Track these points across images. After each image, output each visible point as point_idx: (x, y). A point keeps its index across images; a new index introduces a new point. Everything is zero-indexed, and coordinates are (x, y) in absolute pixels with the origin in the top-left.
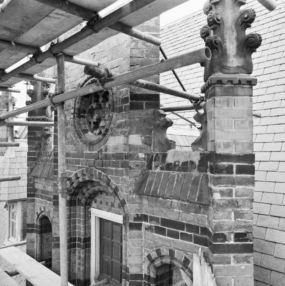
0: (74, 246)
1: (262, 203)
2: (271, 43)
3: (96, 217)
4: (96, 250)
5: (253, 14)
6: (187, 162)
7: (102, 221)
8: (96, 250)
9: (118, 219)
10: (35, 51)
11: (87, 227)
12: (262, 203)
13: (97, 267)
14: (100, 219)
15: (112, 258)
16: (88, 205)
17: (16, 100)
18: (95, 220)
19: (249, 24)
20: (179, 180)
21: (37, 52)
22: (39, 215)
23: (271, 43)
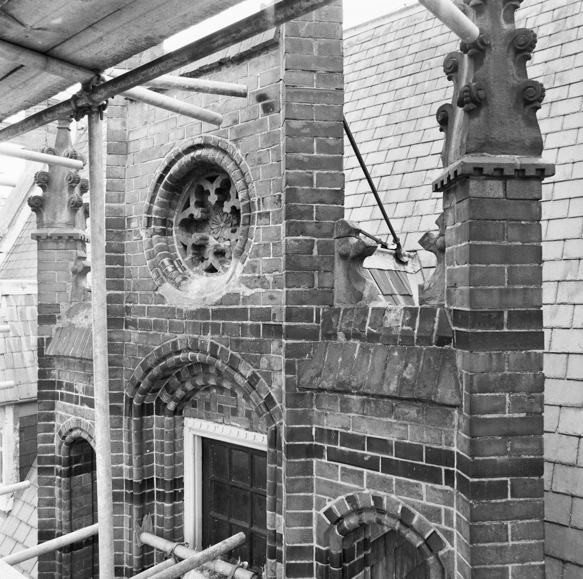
0: (151, 496)
1: (568, 379)
2: (410, 145)
3: (194, 435)
4: (195, 494)
5: (533, 39)
6: (108, 306)
7: (208, 445)
8: (195, 494)
9: (258, 441)
10: (87, 76)
11: (177, 460)
12: (568, 379)
13: (197, 522)
14: (203, 438)
15: (252, 526)
16: (177, 412)
17: (82, 132)
18: (193, 442)
19: (527, 53)
20: (396, 354)
21: (93, 78)
22: (64, 438)
23: (410, 145)
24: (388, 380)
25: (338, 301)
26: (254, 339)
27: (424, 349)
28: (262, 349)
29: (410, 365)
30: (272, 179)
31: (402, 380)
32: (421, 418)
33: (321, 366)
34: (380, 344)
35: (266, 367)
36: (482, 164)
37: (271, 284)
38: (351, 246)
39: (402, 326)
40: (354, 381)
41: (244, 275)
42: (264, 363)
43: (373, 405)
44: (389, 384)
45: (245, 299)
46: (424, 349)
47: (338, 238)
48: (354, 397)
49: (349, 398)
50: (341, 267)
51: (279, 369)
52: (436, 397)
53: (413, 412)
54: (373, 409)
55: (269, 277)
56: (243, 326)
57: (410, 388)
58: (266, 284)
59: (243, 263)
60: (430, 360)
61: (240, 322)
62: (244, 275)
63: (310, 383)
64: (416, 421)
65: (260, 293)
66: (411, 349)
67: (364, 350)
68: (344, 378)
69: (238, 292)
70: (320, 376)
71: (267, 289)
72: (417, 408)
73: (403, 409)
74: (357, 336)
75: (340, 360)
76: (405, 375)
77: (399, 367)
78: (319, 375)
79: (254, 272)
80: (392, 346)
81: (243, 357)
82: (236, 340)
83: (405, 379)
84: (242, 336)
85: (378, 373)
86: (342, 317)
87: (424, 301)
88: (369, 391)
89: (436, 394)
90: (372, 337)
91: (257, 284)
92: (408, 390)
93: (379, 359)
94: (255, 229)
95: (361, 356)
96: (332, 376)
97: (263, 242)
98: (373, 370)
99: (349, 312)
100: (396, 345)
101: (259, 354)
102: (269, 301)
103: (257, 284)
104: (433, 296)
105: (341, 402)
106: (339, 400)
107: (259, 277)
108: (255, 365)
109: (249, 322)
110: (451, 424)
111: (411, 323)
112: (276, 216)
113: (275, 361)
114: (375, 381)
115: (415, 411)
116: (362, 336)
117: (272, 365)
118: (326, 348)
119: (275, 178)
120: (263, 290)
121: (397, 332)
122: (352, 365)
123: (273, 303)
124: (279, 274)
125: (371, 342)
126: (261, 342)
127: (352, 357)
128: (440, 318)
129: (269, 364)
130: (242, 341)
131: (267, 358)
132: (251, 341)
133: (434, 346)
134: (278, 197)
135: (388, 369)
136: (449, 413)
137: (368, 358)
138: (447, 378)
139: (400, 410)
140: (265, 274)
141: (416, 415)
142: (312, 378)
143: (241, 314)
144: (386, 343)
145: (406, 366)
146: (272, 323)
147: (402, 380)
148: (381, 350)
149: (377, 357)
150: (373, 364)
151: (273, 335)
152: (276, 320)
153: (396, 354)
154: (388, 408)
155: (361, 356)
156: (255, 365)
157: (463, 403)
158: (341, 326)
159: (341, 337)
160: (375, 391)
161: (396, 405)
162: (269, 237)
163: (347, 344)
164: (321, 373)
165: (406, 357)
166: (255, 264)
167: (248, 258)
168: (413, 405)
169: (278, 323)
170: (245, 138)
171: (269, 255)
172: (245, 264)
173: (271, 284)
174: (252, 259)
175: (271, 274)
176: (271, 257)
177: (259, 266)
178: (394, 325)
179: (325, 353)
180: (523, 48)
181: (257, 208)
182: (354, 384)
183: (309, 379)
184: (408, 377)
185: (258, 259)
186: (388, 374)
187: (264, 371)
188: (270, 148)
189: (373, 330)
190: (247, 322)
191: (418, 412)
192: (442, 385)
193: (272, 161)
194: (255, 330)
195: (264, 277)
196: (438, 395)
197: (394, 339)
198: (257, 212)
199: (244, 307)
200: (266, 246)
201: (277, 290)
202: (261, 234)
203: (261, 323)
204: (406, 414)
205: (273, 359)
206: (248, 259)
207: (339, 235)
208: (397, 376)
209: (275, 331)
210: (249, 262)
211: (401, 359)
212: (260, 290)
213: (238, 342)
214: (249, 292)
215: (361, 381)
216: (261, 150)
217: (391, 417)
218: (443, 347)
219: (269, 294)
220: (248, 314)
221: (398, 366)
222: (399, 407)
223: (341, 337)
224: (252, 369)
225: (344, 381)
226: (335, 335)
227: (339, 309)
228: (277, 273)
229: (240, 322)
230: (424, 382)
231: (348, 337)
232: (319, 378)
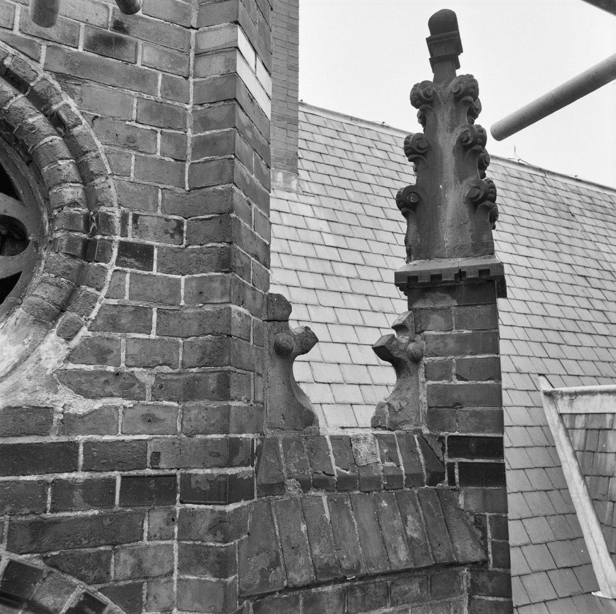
20: (384, 504)
24: (391, 546)
25: (272, 427)
26: (96, 512)
27: (416, 492)
28: (121, 533)
29: (410, 518)
30: (161, 186)
31: (409, 541)
32: (425, 593)
33: (274, 544)
34: (358, 492)
35: (129, 573)
36: (441, 270)
37: (148, 391)
38: (294, 336)
39: (383, 462)
40: (343, 559)
41: (71, 366)
42: (121, 567)
43: (359, 594)
44: (396, 552)
45: (70, 422)
46: (416, 492)
47: (268, 321)
48: (329, 589)
49: (320, 593)
50: (277, 369)
51: (167, 569)
52: (457, 555)
53: (414, 588)
54: (360, 600)
55: (146, 377)
56: (58, 485)
57: (424, 551)
58: (136, 390)
59: (68, 339)
60: (429, 506)
61: (49, 478)
62: (71, 366)
63: (264, 583)
64: (420, 600)
65: (117, 408)
66: (400, 493)
67: (337, 505)
68: (325, 558)
69: (48, 403)
70: (278, 564)
71: (138, 399)
72: (420, 580)
73: (402, 587)
74: (322, 483)
75: (303, 528)
76: (409, 533)
77: (397, 523)
78: (275, 564)
79: (103, 360)
80: (375, 492)
81: (54, 564)
82: (32, 524)
83: (412, 539)
84: (52, 511)
85: (374, 538)
86: (285, 454)
87: (397, 426)
88: (373, 570)
89: (455, 550)
90: (345, 484)
91: (109, 389)
92: (422, 554)
93: (366, 516)
94: (110, 272)
95: (337, 516)
96: (301, 560)
97: (133, 303)
98: (364, 537)
99: (293, 445)
100: (379, 491)
101: (109, 548)
102: (142, 426)
103: (109, 389)
104: (408, 419)
105: (305, 603)
106: (301, 602)
107: (117, 374)
108: (92, 575)
109: (80, 476)
110: (460, 589)
111: (392, 458)
112: (169, 257)
113: (155, 556)
114: (375, 551)
115: (417, 585)
116: (331, 483)
117: (146, 565)
118: (270, 510)
119: (168, 187)
120: (128, 403)
121: (378, 471)
122: (328, 534)
123: (154, 430)
124: (171, 370)
125: (345, 491)
126: (118, 518)
127: (322, 519)
128: (422, 447)
129: (139, 566)
130: (56, 522)
131: (132, 553)
132: (86, 519)
133: (426, 486)
134: (175, 224)
135: (384, 528)
136: (456, 574)
137: (349, 516)
138: (460, 529)
139: (397, 589)
140: (135, 369)
141: (419, 590)
142: (264, 573)
143: (64, 456)
144: (367, 490)
145: (405, 520)
146: (149, 471)
147: (409, 541)
148: (363, 500)
149: (361, 518)
150: (360, 525)
151: (151, 499)
152: (162, 465)
153: (386, 505)
154: (381, 592)
155: (337, 516)
156: (92, 575)
157: (490, 556)
158: (288, 470)
159: (293, 488)
160: (380, 569)
161: (392, 583)
162: (148, 293)
163: (305, 497)
164: (277, 558)
165: (399, 506)
166: (106, 344)
167: (85, 329)
168: (415, 577)
169: (167, 472)
170: (92, 84)
171: (148, 330)
172: (75, 342)
173: (148, 391)
174: (98, 334)
175: (149, 371)
176: (153, 336)
177: (119, 350)
178: (371, 461)
179: (272, 520)
180: (421, 152)
181: (118, 230)
182: (346, 565)
183: (259, 577)
184: (415, 535)
185: (117, 335)
186: (388, 538)
187: (122, 583)
188: (159, 130)
189: (345, 471)
190: (73, 475)
191: (421, 585)
192: (456, 538)
193: (163, 154)
194: (99, 493)
195: (132, 375)
196: (459, 552)
197: (374, 482)
198: (118, 238)
199: (63, 439)
200: (140, 314)
201: (166, 403)
202: (127, 286)
203: (117, 475)
204: (406, 593)
205: (151, 553)
206: (84, 332)
207: (271, 317)
208: (400, 538)
209: (160, 491)
210: (87, 340)
211: (394, 509)
212: (118, 402)
213: (39, 528)
214: (82, 406)
215: (354, 557)
216: (134, 124)
217: (386, 605)
218: (435, 486)
219: (144, 411)
220: (77, 457)
221: (395, 522)
222: (397, 585)
223: (293, 488)
224: (81, 588)
225: (328, 564)
226: (282, 486)
227: (275, 440)
228: (166, 369)
229: (49, 478)
230: (435, 538)
231: (305, 486)
232: (278, 569)
